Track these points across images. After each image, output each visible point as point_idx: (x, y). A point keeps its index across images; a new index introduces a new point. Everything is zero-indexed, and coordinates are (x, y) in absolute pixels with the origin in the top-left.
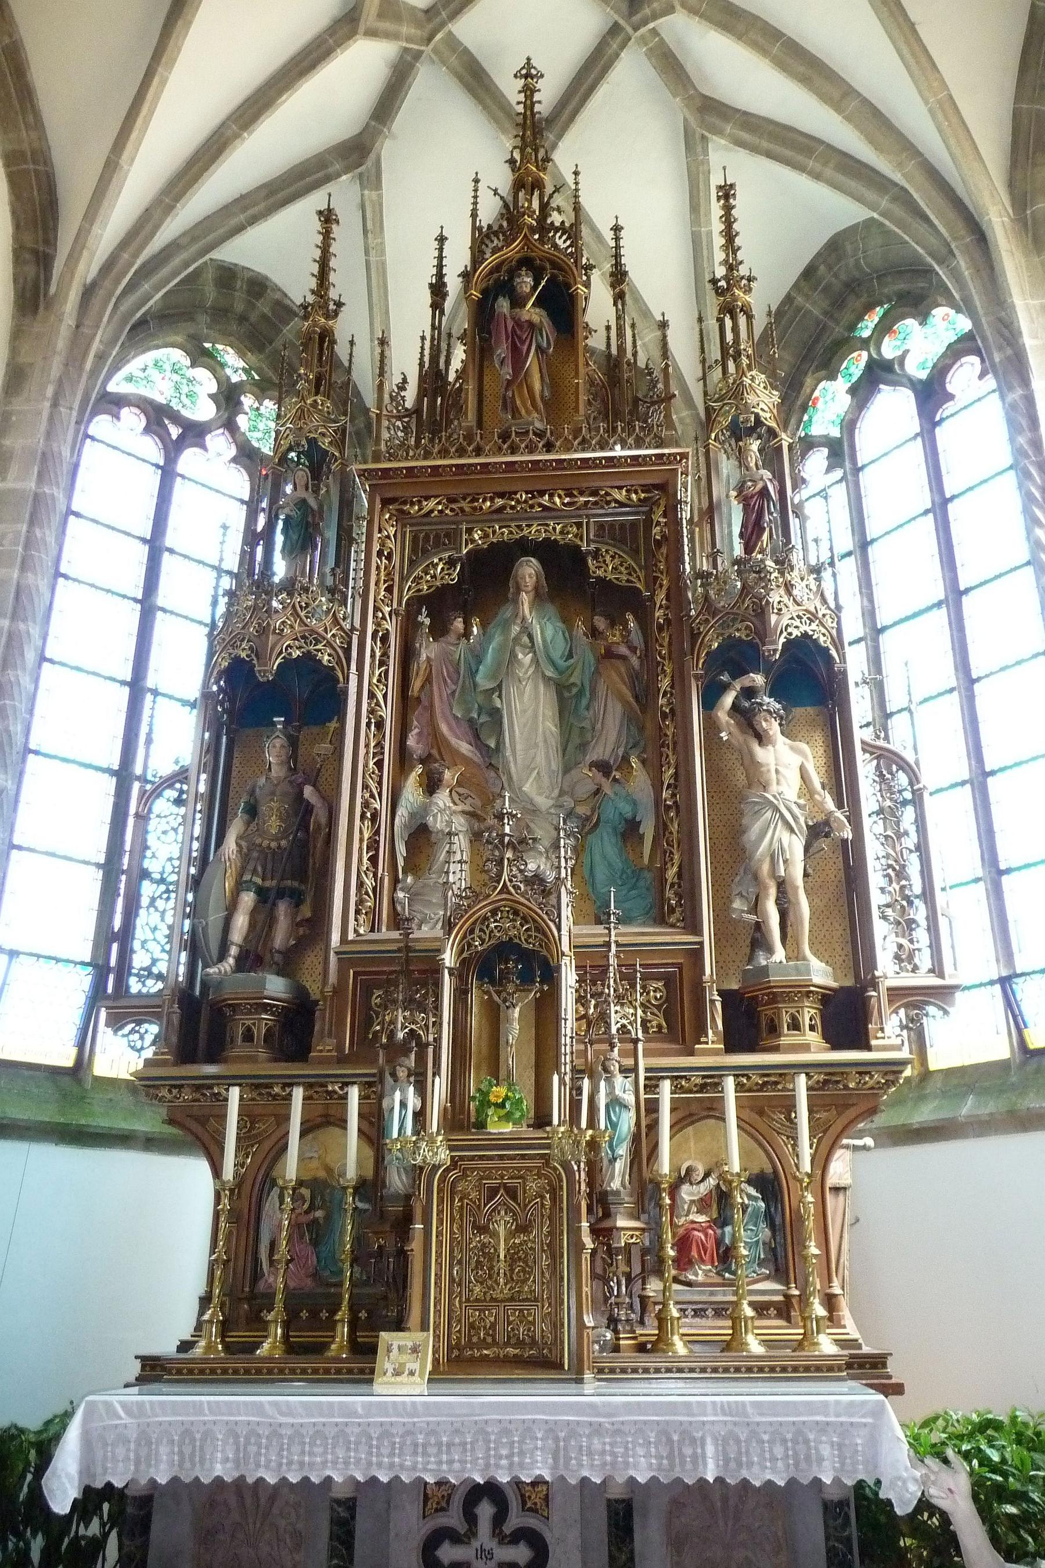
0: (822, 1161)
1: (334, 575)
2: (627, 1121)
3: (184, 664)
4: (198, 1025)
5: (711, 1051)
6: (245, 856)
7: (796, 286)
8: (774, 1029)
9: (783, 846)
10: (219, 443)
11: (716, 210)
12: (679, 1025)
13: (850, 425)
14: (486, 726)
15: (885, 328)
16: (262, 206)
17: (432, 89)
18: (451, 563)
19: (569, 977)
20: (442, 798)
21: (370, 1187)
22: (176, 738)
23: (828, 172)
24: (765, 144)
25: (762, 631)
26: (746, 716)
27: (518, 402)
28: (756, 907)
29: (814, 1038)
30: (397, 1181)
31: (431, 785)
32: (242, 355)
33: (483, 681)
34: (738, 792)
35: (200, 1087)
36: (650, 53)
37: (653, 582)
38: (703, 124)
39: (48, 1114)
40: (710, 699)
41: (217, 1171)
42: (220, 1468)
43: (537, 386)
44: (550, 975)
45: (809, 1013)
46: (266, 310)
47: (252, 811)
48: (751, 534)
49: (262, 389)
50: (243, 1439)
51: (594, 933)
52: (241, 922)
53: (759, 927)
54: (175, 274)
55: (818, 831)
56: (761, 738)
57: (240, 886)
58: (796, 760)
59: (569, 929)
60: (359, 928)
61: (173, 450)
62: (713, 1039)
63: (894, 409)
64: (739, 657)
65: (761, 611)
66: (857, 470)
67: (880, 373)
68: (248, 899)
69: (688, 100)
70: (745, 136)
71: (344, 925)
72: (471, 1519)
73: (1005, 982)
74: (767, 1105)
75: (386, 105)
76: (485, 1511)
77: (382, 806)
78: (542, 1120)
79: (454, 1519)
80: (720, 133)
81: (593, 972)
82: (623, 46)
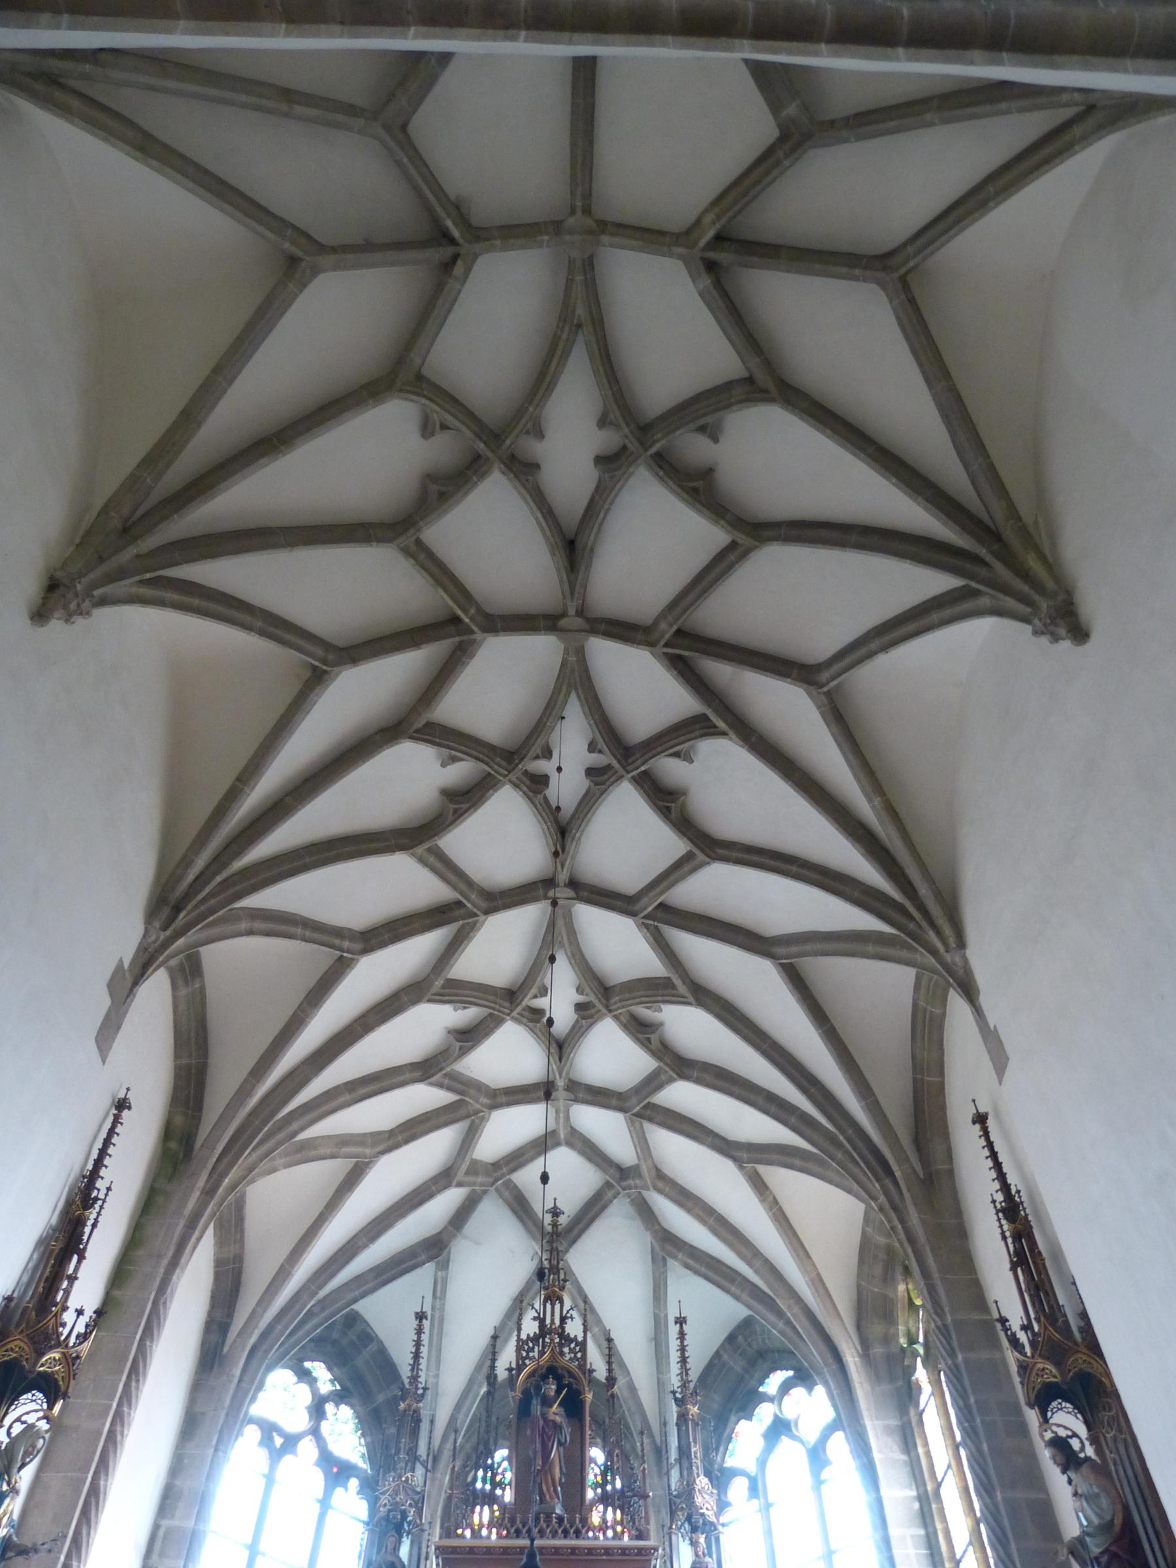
7: (722, 1346)
10: (308, 1449)
11: (674, 1330)
13: (762, 1463)
15: (785, 1388)
16: (370, 1285)
17: (492, 1215)
23: (745, 1296)
24: (703, 1269)
27: (544, 1488)
32: (330, 1369)
36: (633, 1202)
38: (663, 1249)
43: (557, 1475)
46: (354, 1338)
49: (340, 1397)
54: (308, 1334)
61: (276, 1455)
63: (790, 1455)
66: (768, 1506)
67: (780, 1428)
69: (655, 1233)
70: (691, 1262)
75: (460, 1218)
80: (674, 1257)
82: (615, 1197)
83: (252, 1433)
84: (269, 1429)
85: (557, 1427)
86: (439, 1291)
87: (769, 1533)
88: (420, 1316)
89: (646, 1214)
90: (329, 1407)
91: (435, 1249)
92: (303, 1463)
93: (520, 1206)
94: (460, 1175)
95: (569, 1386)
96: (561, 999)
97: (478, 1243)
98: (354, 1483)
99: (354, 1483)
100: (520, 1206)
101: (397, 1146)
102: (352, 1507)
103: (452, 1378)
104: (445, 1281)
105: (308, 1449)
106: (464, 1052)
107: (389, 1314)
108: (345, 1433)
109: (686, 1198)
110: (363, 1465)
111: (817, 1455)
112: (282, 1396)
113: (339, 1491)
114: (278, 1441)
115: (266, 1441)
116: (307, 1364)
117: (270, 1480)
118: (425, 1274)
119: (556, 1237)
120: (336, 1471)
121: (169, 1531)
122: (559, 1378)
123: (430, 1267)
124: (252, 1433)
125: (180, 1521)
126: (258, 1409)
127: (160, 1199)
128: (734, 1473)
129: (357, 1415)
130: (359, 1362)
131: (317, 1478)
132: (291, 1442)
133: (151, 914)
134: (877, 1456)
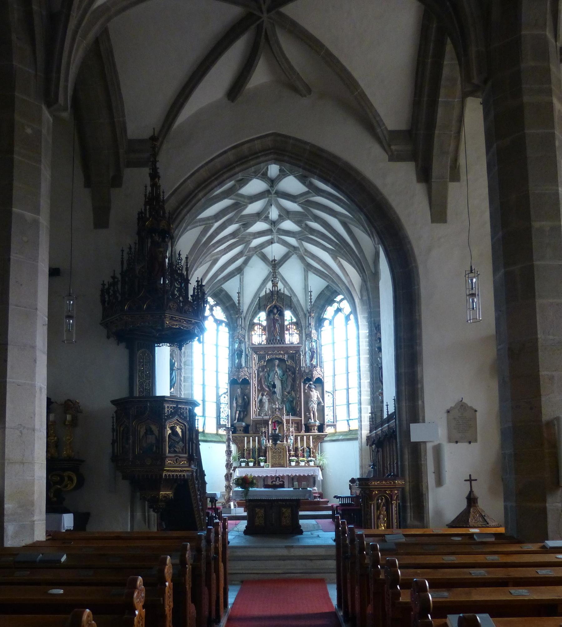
1: (406, 585)
4: (234, 429)
8: (311, 430)
12: (298, 429)
13: (333, 318)
18: (265, 361)
20: (264, 397)
21: (260, 449)
25: (312, 377)
26: (309, 388)
29: (316, 431)
31: (263, 395)
34: (308, 398)
37: (296, 366)
40: (305, 383)
45: (316, 428)
47: (236, 399)
48: (312, 358)
49: (216, 305)
52: (237, 415)
53: (310, 417)
55: (319, 404)
56: (312, 391)
57: (236, 410)
58: (316, 394)
59: (285, 418)
62: (303, 431)
63: (341, 317)
64: (309, 380)
65: (312, 374)
66: (334, 328)
67: (339, 310)
68: (238, 412)
72: (276, 480)
73: (348, 421)
76: (278, 479)
77: (256, 399)
79: (274, 480)
85: (277, 320)
86: (241, 281)
87: (333, 334)
88: (238, 293)
89: (302, 259)
90: (214, 308)
91: (239, 270)
93: (264, 258)
95: (280, 310)
96: (274, 214)
97: (252, 267)
98: (224, 324)
104: (243, 278)
106: (241, 187)
109: (314, 257)
110: (225, 320)
111: (347, 318)
118: (237, 277)
119: (275, 265)
120: (218, 322)
122: (277, 308)
123: (238, 276)
128: (326, 319)
129: (222, 309)
130: (221, 296)
134: (360, 323)
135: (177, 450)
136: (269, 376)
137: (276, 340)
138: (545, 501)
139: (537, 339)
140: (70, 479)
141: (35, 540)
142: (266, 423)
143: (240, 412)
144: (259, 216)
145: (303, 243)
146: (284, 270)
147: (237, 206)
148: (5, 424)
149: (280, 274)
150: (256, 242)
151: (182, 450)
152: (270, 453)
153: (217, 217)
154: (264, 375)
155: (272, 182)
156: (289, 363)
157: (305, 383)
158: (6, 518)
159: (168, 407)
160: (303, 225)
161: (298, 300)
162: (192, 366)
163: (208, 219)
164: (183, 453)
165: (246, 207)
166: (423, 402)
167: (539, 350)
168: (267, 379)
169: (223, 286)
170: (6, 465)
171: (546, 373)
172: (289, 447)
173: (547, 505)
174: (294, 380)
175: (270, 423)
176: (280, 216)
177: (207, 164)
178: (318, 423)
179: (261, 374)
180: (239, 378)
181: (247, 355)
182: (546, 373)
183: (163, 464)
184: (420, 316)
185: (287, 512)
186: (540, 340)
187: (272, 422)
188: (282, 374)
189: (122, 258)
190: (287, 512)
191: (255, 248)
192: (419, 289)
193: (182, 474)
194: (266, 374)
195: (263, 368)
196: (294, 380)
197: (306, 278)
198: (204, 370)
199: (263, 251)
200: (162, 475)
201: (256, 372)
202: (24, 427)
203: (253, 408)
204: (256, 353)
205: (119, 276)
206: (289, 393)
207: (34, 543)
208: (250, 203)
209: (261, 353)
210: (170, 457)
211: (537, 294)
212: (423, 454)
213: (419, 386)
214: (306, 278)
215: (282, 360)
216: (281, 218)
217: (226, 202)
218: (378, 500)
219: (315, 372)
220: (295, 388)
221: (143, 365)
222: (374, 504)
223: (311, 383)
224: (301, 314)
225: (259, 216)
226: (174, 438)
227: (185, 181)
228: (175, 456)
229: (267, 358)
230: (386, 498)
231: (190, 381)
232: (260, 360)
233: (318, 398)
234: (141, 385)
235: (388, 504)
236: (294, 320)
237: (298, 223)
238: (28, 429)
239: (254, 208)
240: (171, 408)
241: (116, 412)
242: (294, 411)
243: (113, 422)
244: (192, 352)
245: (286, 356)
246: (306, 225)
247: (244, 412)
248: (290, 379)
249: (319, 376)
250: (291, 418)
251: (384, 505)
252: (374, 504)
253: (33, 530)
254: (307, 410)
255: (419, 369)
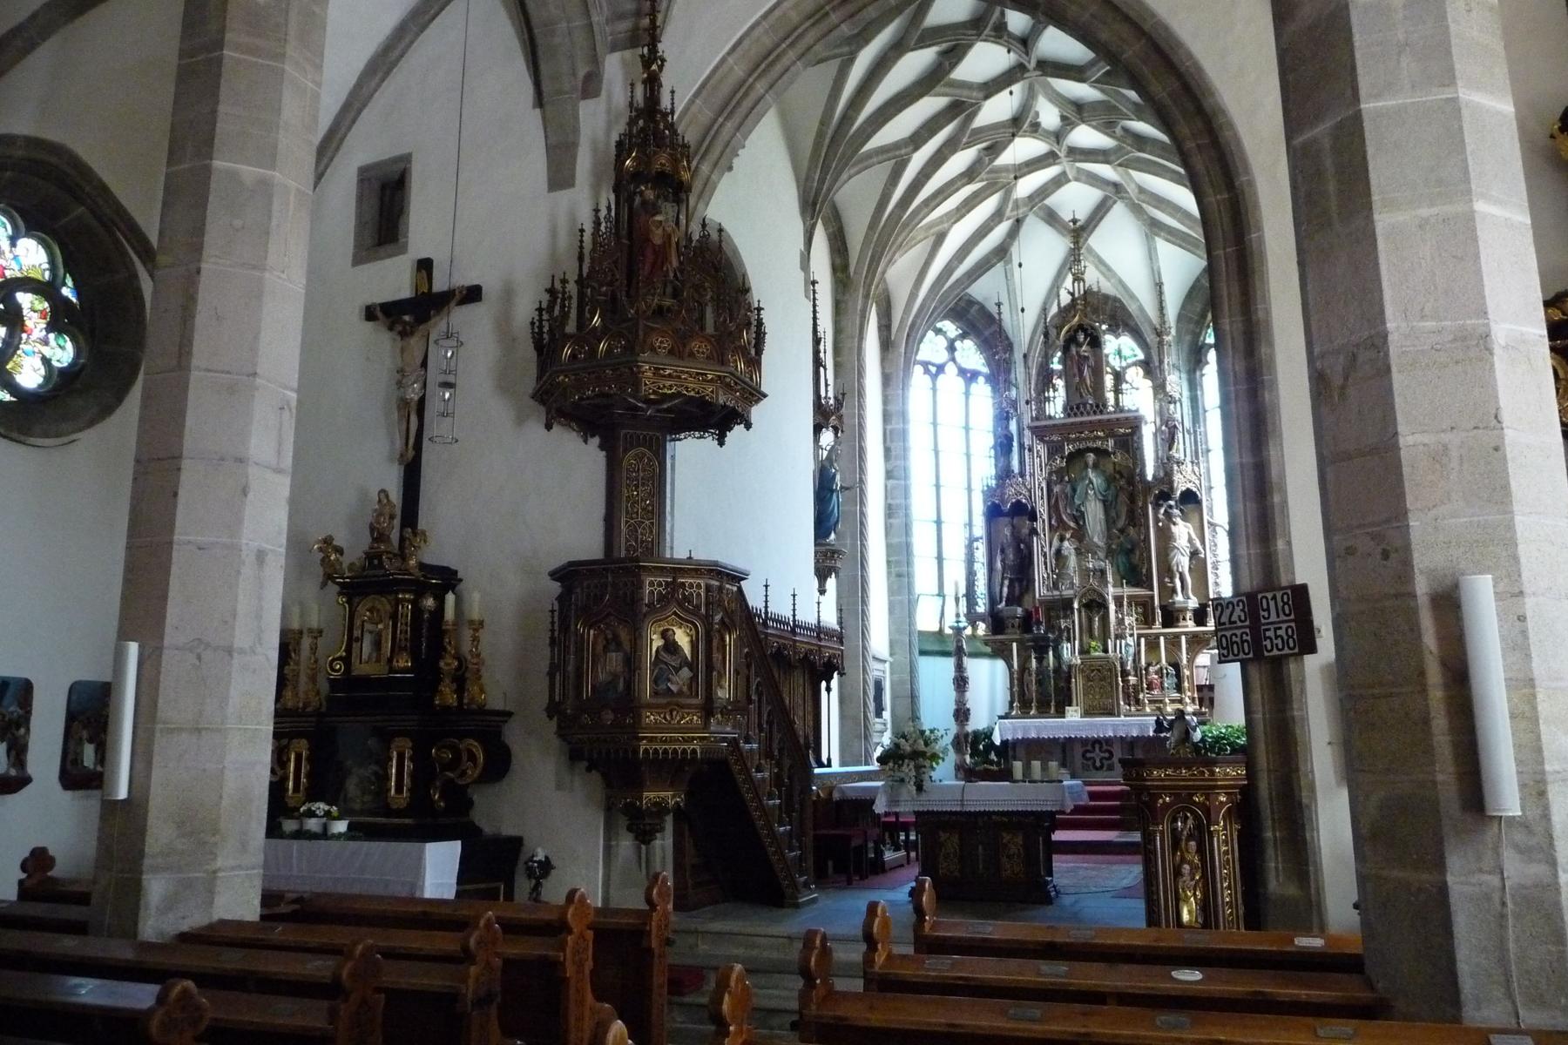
0: (1191, 661)
2: (1132, 650)
3: (979, 508)
5: (1157, 628)
6: (1004, 568)
9: (1182, 561)
10: (951, 369)
12: (1147, 619)
14: (1079, 518)
19: (1112, 607)
20: (1066, 544)
21: (1058, 670)
22: (979, 529)
25: (1172, 489)
28: (1172, 581)
30: (1065, 668)
31: (1062, 539)
33: (1077, 502)
34: (1166, 537)
35: (1001, 642)
39: (936, 648)
40: (1157, 506)
41: (1010, 666)
42: (1033, 735)
44: (1107, 608)
45: (1189, 615)
47: (1003, 551)
49: (963, 337)
50: (1038, 729)
51: (1119, 591)
52: (1005, 590)
55: (1194, 554)
57: (1003, 578)
59: (1111, 591)
60: (1044, 591)
61: (934, 377)
64: (1166, 496)
65: (1171, 482)
71: (1041, 590)
74: (1174, 642)
75: (1013, 234)
77: (1047, 549)
78: (1106, 651)
81: (1119, 601)
83: (918, 369)
84: (925, 364)
85: (1086, 358)
86: (1008, 276)
89: (1137, 210)
90: (958, 344)
91: (1002, 252)
92: (951, 376)
93: (1051, 218)
94: (1008, 212)
96: (1049, 116)
98: (981, 379)
99: (981, 379)
100: (1051, 218)
101: (963, 216)
102: (982, 391)
103: (1023, 327)
105: (951, 369)
106: (953, 66)
107: (985, 290)
108: (971, 355)
110: (985, 370)
112: (932, 348)
113: (974, 386)
114: (933, 369)
115: (927, 371)
116: (939, 325)
117: (934, 389)
119: (1078, 233)
120: (969, 376)
121: (892, 432)
122: (1085, 331)
123: (1000, 265)
124: (918, 369)
125: (895, 425)
126: (921, 356)
127: (843, 306)
131: (960, 382)
132: (941, 368)
133: (803, 212)
135: (674, 688)
136: (1074, 490)
137: (1085, 405)
138: (1440, 865)
139: (1384, 336)
140: (472, 757)
141: (216, 917)
142: (1066, 605)
143: (1011, 581)
144: (1019, 123)
145: (1132, 172)
146: (1098, 241)
147: (961, 109)
148: (162, 638)
149: (1090, 250)
150: (1027, 186)
151: (690, 688)
152: (1080, 682)
153: (917, 139)
154: (1063, 491)
155: (1025, 42)
156: (1117, 458)
157: (1157, 506)
158: (147, 862)
159: (652, 584)
160: (1118, 130)
161: (1141, 309)
162: (906, 478)
163: (896, 146)
164: (690, 696)
165: (979, 109)
166: (1289, 543)
167: (1394, 369)
168: (1070, 500)
169: (969, 291)
170: (158, 735)
171: (1419, 438)
172: (1123, 665)
173: (1450, 879)
174: (1132, 499)
175: (1076, 606)
176: (1063, 118)
177: (765, 16)
178: (1193, 603)
179: (1057, 489)
180: (1003, 501)
181: (1021, 446)
182: (1419, 438)
183: (637, 724)
184: (1268, 312)
185: (1014, 842)
186: (1393, 339)
187: (1082, 605)
188: (1104, 485)
189: (581, 247)
190: (1014, 842)
191: (1031, 197)
192: (1261, 240)
193: (661, 747)
194: (1068, 489)
195: (1060, 473)
196: (1132, 499)
197: (1152, 255)
198: (938, 486)
199: (1047, 202)
200: (636, 752)
201: (1044, 485)
202: (208, 645)
203: (1040, 572)
204: (1042, 440)
205: (572, 288)
206: (1122, 531)
207: (211, 927)
208: (987, 97)
209: (1055, 438)
210: (658, 706)
211: (1375, 198)
212: (1296, 690)
213: (1276, 499)
214: (1152, 255)
215: (1101, 453)
216: (1068, 123)
217: (929, 105)
218: (1175, 820)
219: (1177, 478)
220: (1136, 519)
221: (637, 486)
222: (1162, 833)
223: (1172, 503)
224: (1151, 338)
225: (1019, 123)
226: (665, 657)
227: (723, 60)
228: (669, 704)
229: (1068, 449)
230: (1196, 817)
231: (902, 513)
232: (1051, 455)
233: (1190, 540)
234: (633, 531)
235: (1202, 835)
236: (1141, 356)
237: (1107, 127)
238: (216, 649)
239: (998, 108)
240: (660, 584)
241: (560, 598)
242: (1134, 574)
243: (553, 623)
244: (905, 449)
245: (1111, 442)
246: (1125, 130)
247: (1020, 581)
248: (1123, 498)
249: (1190, 486)
250: (1128, 591)
251: (1190, 837)
252: (1162, 833)
253: (211, 892)
254: (1167, 570)
255: (1273, 453)
